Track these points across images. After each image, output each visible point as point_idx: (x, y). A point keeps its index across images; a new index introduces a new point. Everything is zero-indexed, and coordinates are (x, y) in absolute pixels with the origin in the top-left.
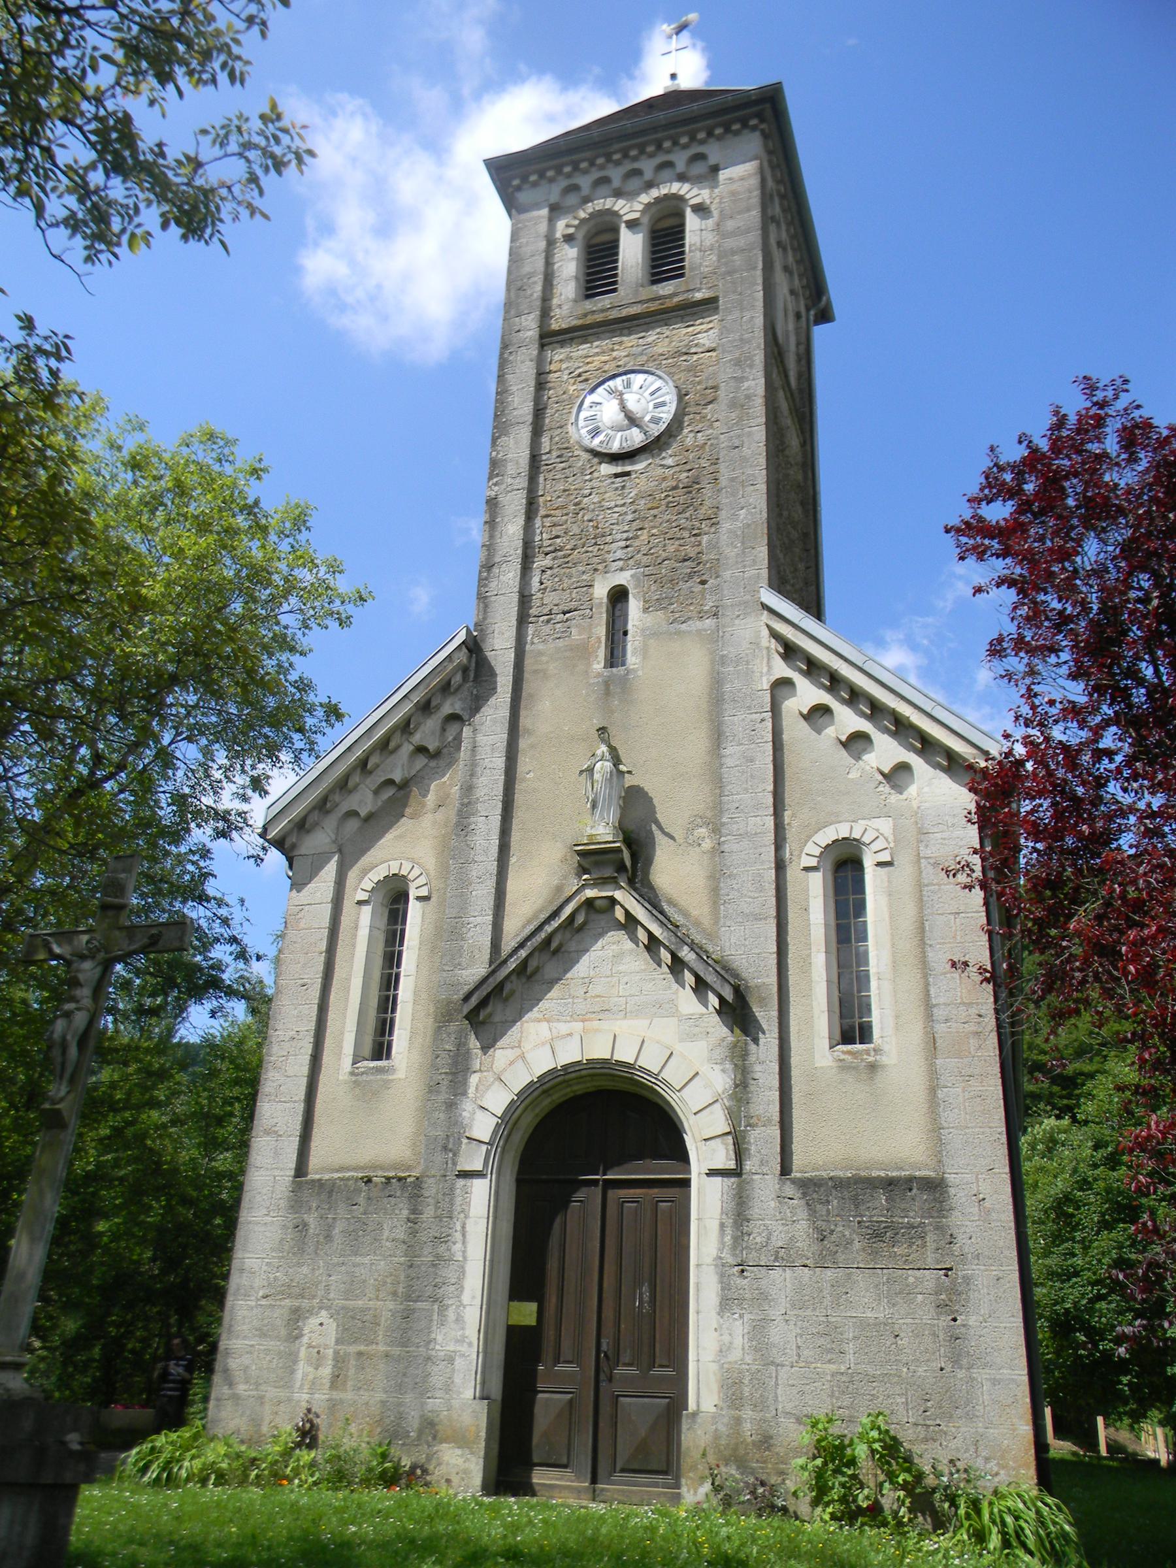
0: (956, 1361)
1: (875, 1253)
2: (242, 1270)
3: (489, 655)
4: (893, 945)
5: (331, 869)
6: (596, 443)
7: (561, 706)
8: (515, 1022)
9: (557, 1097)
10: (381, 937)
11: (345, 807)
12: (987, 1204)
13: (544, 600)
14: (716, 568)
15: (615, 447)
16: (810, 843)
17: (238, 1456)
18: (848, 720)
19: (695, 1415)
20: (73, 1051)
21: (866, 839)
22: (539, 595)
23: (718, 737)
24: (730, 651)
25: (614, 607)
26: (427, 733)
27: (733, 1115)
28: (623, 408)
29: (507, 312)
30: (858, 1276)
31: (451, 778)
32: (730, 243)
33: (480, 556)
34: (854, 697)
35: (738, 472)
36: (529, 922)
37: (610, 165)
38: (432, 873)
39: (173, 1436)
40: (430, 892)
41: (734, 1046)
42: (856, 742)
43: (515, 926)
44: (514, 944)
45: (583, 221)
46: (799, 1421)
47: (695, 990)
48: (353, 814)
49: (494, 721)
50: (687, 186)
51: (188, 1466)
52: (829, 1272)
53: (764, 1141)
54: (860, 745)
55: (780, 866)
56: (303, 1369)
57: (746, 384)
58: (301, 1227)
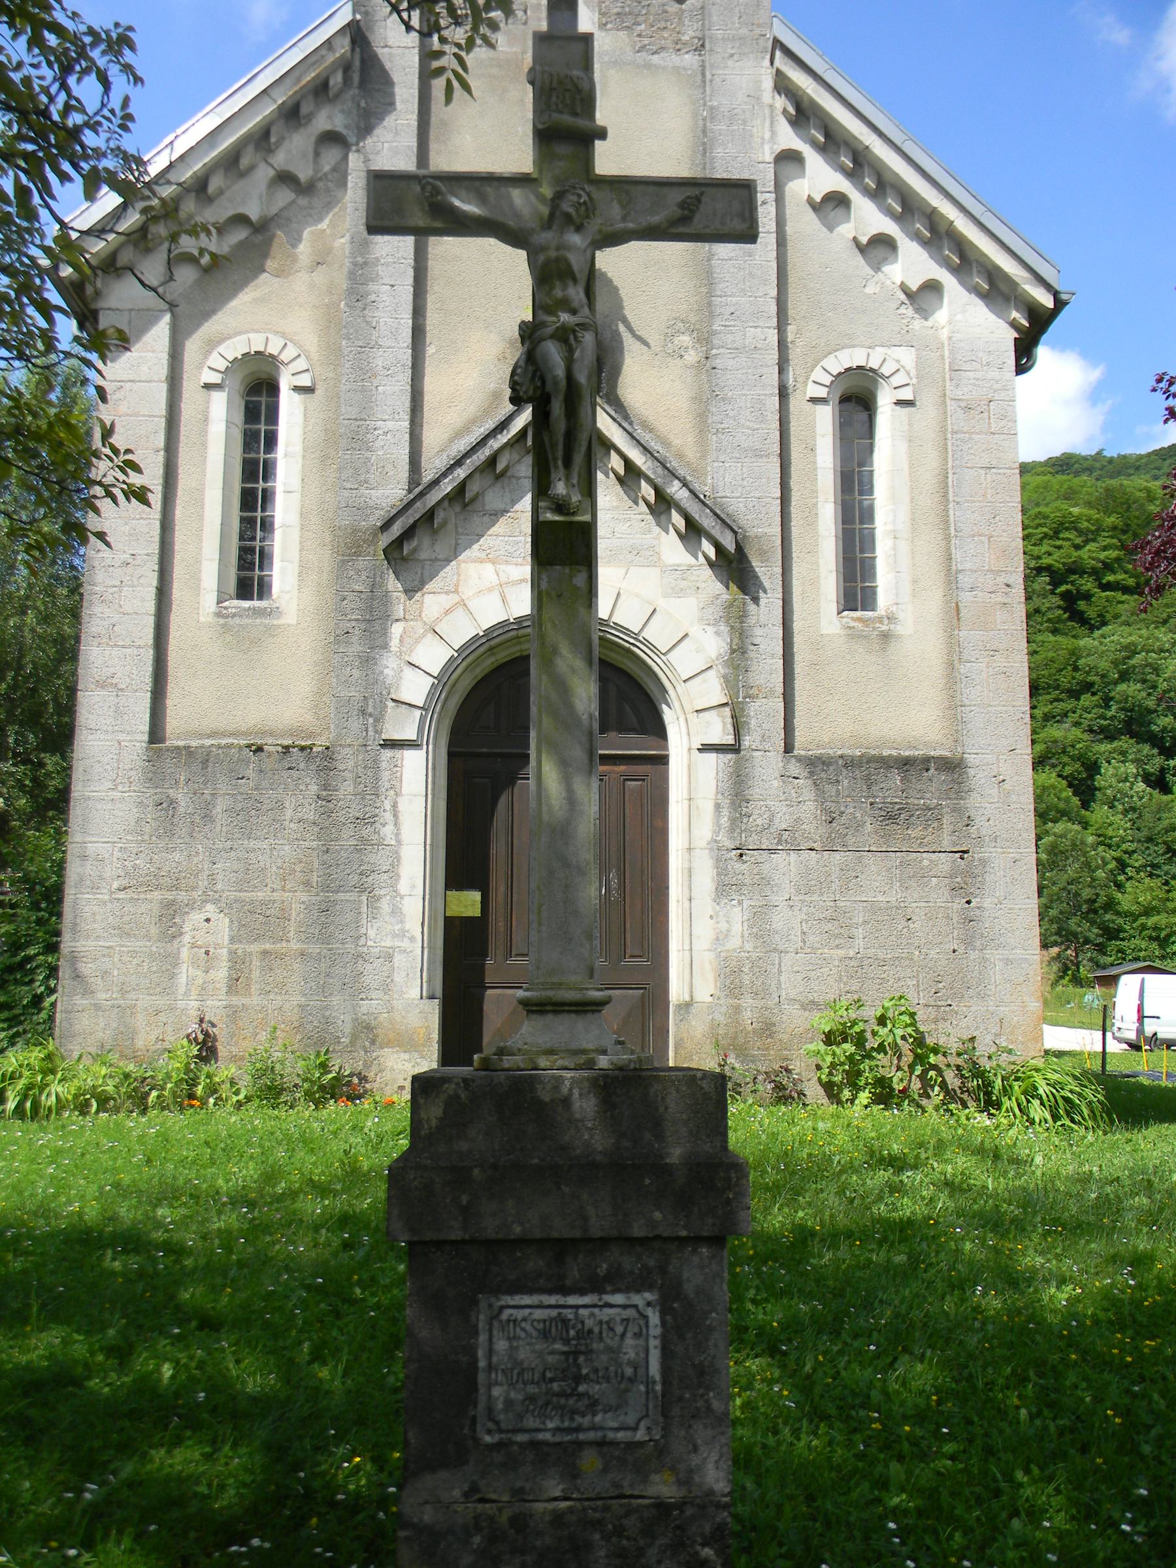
0: (968, 942)
3: (382, 53)
8: (448, 561)
12: (1006, 786)
16: (818, 369)
19: (686, 1006)
26: (294, 151)
30: (869, 859)
31: (332, 225)
36: (458, 435)
38: (315, 356)
40: (313, 380)
41: (730, 605)
42: (878, 247)
44: (441, 463)
46: (804, 1007)
52: (837, 856)
53: (765, 714)
54: (880, 252)
55: (783, 393)
58: (166, 806)
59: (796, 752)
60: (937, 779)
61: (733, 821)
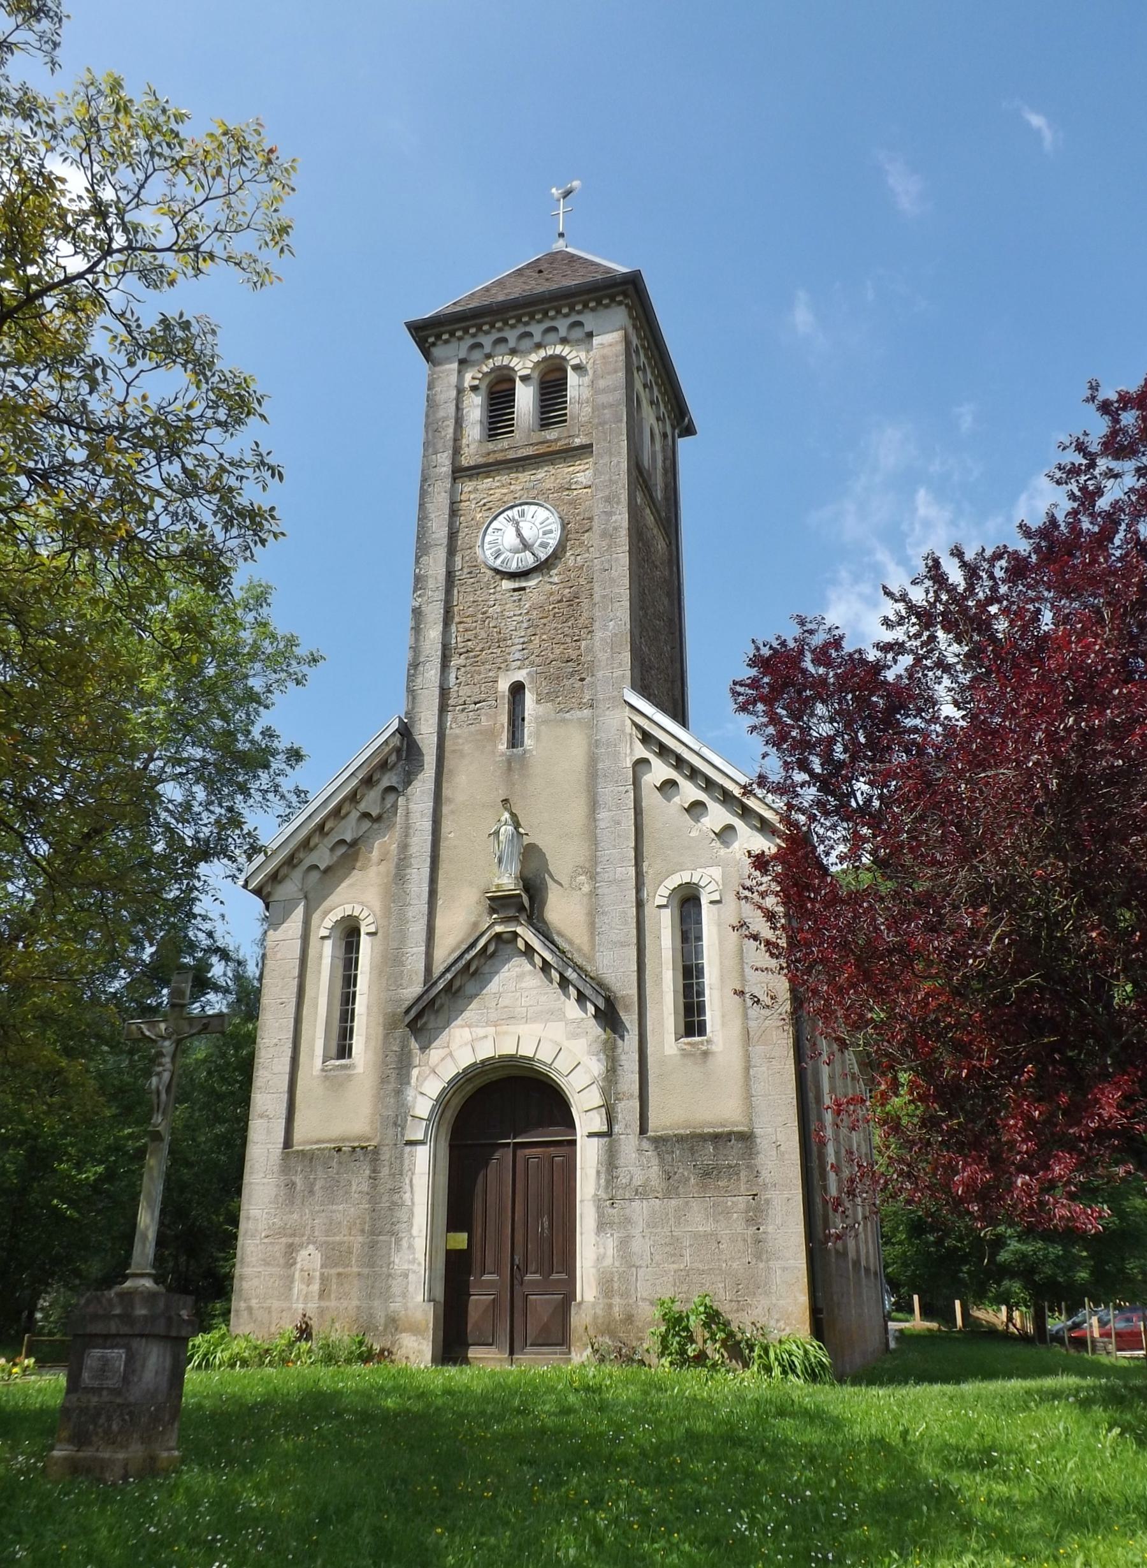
0: (758, 1257)
1: (704, 1187)
2: (248, 1218)
4: (721, 963)
5: (299, 912)
6: (497, 564)
7: (474, 779)
9: (479, 1082)
10: (340, 965)
11: (308, 862)
12: (782, 1148)
13: (460, 693)
14: (591, 670)
15: (513, 567)
17: (256, 1348)
18: (690, 792)
19: (580, 1304)
20: (163, 1096)
21: (702, 884)
22: (456, 688)
23: (594, 805)
24: (602, 736)
25: (514, 697)
26: (371, 802)
27: (605, 1092)
28: (519, 534)
29: (425, 450)
32: (603, 399)
33: (408, 656)
34: (694, 774)
35: (608, 591)
36: (453, 951)
37: (507, 328)
38: (378, 913)
39: (208, 1337)
41: (606, 1042)
42: (696, 809)
43: (443, 954)
44: (442, 969)
45: (485, 374)
46: (652, 1304)
47: (578, 1001)
48: (315, 867)
49: (423, 792)
50: (567, 349)
51: (221, 1355)
53: (628, 1110)
54: (699, 810)
55: (640, 905)
56: (298, 1286)
57: (614, 518)
58: (291, 1185)
59: (650, 1134)
60: (737, 1146)
61: (608, 1182)
